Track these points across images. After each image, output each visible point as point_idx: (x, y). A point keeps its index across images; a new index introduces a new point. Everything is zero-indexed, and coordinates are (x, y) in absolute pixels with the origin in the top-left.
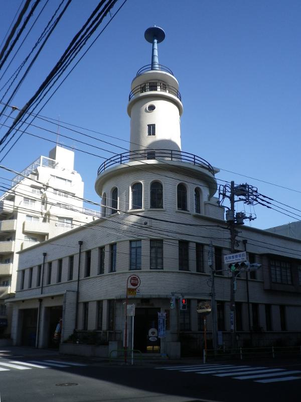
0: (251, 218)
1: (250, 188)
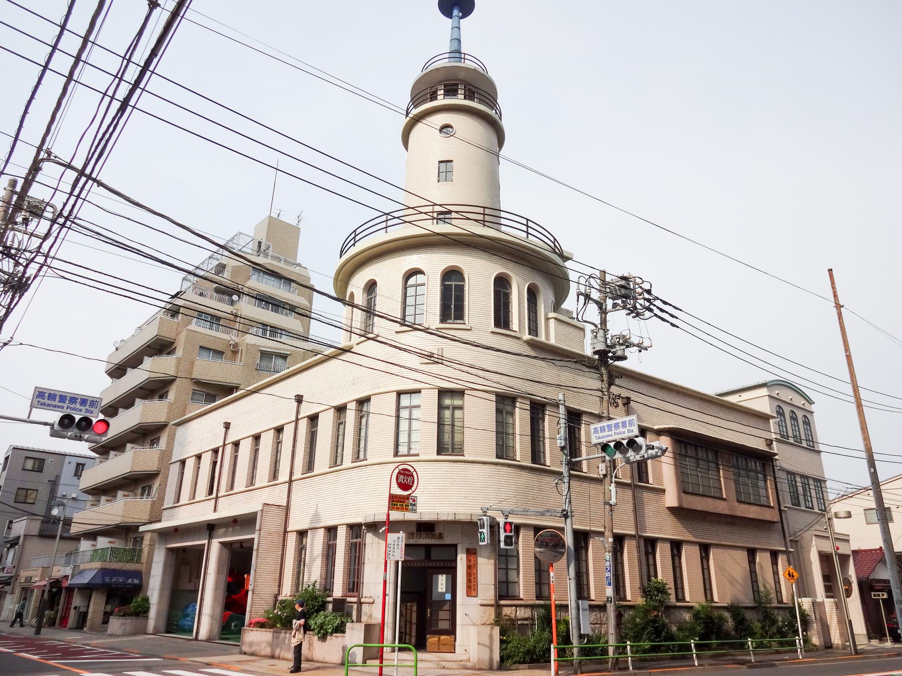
0: (641, 347)
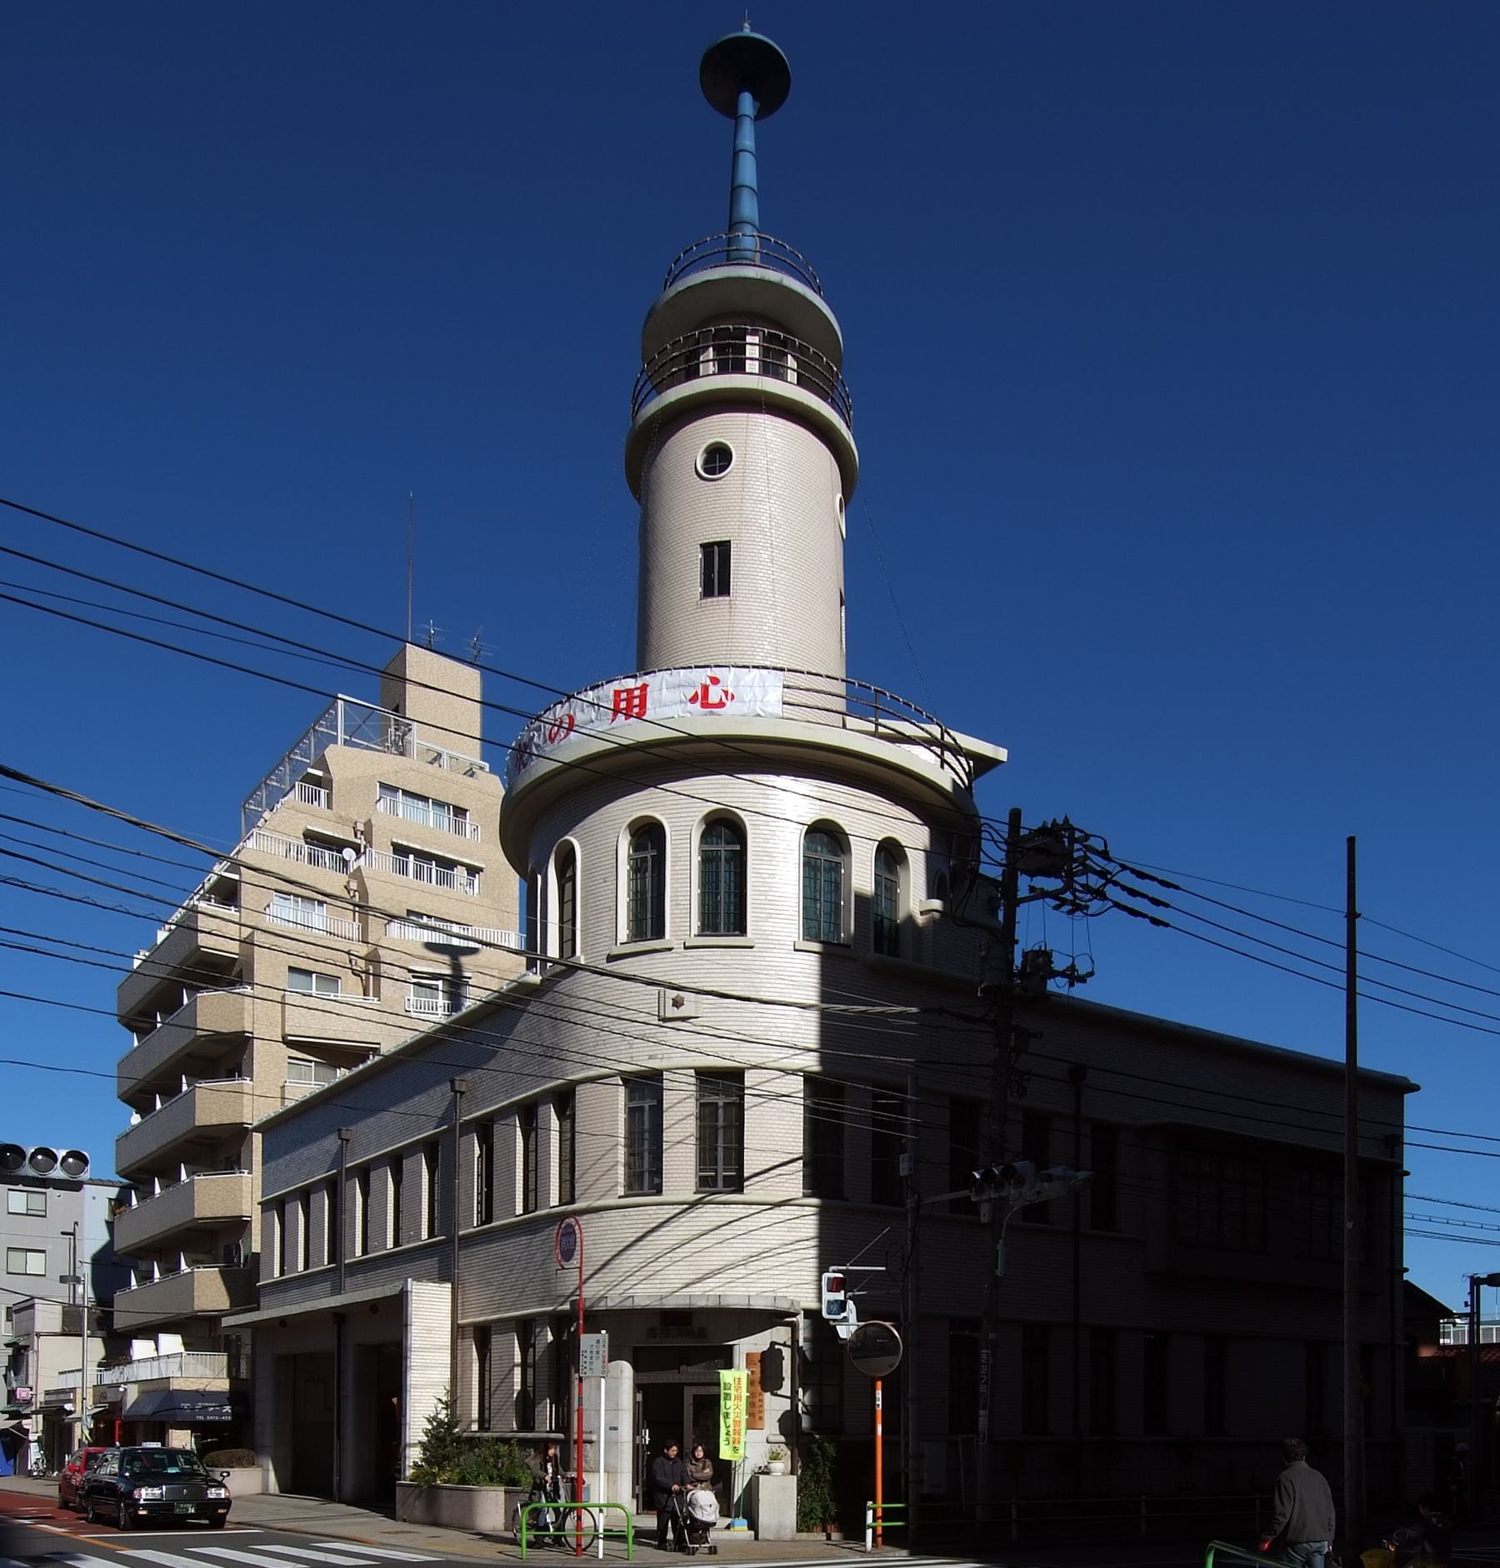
1: (1077, 841)
